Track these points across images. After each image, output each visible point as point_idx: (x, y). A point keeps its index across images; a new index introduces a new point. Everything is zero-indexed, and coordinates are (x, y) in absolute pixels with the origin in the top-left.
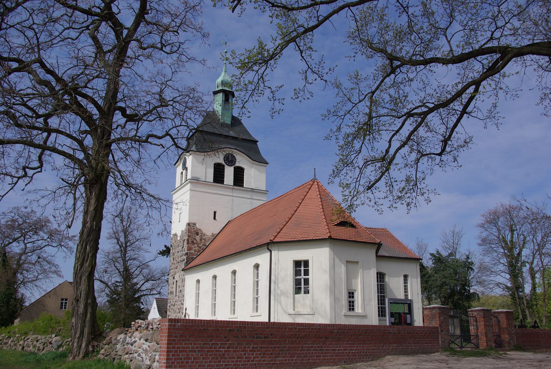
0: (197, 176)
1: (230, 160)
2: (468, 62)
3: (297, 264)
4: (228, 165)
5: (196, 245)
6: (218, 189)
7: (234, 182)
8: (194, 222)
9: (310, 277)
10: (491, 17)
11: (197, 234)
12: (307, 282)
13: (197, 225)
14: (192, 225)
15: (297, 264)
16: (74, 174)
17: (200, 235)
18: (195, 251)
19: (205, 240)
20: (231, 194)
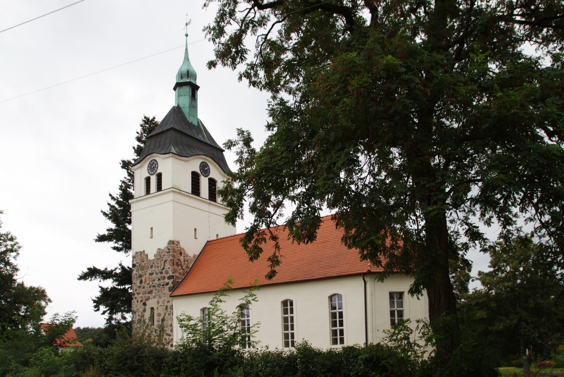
0: (178, 185)
1: (204, 168)
2: (452, 222)
3: (285, 303)
4: (203, 175)
5: (180, 267)
6: (193, 202)
7: (192, 188)
8: (177, 239)
9: (344, 328)
10: (478, 277)
11: (181, 254)
12: (342, 332)
13: (181, 244)
14: (176, 243)
15: (285, 303)
16: (274, 261)
17: (183, 255)
18: (180, 273)
19: (187, 261)
20: (207, 209)
